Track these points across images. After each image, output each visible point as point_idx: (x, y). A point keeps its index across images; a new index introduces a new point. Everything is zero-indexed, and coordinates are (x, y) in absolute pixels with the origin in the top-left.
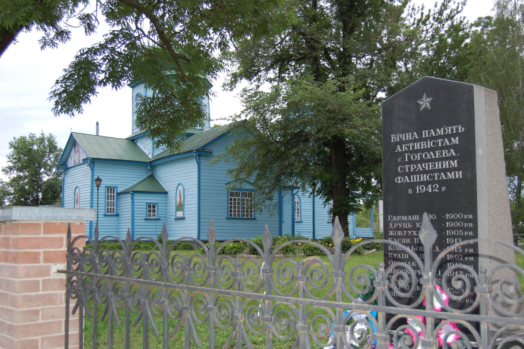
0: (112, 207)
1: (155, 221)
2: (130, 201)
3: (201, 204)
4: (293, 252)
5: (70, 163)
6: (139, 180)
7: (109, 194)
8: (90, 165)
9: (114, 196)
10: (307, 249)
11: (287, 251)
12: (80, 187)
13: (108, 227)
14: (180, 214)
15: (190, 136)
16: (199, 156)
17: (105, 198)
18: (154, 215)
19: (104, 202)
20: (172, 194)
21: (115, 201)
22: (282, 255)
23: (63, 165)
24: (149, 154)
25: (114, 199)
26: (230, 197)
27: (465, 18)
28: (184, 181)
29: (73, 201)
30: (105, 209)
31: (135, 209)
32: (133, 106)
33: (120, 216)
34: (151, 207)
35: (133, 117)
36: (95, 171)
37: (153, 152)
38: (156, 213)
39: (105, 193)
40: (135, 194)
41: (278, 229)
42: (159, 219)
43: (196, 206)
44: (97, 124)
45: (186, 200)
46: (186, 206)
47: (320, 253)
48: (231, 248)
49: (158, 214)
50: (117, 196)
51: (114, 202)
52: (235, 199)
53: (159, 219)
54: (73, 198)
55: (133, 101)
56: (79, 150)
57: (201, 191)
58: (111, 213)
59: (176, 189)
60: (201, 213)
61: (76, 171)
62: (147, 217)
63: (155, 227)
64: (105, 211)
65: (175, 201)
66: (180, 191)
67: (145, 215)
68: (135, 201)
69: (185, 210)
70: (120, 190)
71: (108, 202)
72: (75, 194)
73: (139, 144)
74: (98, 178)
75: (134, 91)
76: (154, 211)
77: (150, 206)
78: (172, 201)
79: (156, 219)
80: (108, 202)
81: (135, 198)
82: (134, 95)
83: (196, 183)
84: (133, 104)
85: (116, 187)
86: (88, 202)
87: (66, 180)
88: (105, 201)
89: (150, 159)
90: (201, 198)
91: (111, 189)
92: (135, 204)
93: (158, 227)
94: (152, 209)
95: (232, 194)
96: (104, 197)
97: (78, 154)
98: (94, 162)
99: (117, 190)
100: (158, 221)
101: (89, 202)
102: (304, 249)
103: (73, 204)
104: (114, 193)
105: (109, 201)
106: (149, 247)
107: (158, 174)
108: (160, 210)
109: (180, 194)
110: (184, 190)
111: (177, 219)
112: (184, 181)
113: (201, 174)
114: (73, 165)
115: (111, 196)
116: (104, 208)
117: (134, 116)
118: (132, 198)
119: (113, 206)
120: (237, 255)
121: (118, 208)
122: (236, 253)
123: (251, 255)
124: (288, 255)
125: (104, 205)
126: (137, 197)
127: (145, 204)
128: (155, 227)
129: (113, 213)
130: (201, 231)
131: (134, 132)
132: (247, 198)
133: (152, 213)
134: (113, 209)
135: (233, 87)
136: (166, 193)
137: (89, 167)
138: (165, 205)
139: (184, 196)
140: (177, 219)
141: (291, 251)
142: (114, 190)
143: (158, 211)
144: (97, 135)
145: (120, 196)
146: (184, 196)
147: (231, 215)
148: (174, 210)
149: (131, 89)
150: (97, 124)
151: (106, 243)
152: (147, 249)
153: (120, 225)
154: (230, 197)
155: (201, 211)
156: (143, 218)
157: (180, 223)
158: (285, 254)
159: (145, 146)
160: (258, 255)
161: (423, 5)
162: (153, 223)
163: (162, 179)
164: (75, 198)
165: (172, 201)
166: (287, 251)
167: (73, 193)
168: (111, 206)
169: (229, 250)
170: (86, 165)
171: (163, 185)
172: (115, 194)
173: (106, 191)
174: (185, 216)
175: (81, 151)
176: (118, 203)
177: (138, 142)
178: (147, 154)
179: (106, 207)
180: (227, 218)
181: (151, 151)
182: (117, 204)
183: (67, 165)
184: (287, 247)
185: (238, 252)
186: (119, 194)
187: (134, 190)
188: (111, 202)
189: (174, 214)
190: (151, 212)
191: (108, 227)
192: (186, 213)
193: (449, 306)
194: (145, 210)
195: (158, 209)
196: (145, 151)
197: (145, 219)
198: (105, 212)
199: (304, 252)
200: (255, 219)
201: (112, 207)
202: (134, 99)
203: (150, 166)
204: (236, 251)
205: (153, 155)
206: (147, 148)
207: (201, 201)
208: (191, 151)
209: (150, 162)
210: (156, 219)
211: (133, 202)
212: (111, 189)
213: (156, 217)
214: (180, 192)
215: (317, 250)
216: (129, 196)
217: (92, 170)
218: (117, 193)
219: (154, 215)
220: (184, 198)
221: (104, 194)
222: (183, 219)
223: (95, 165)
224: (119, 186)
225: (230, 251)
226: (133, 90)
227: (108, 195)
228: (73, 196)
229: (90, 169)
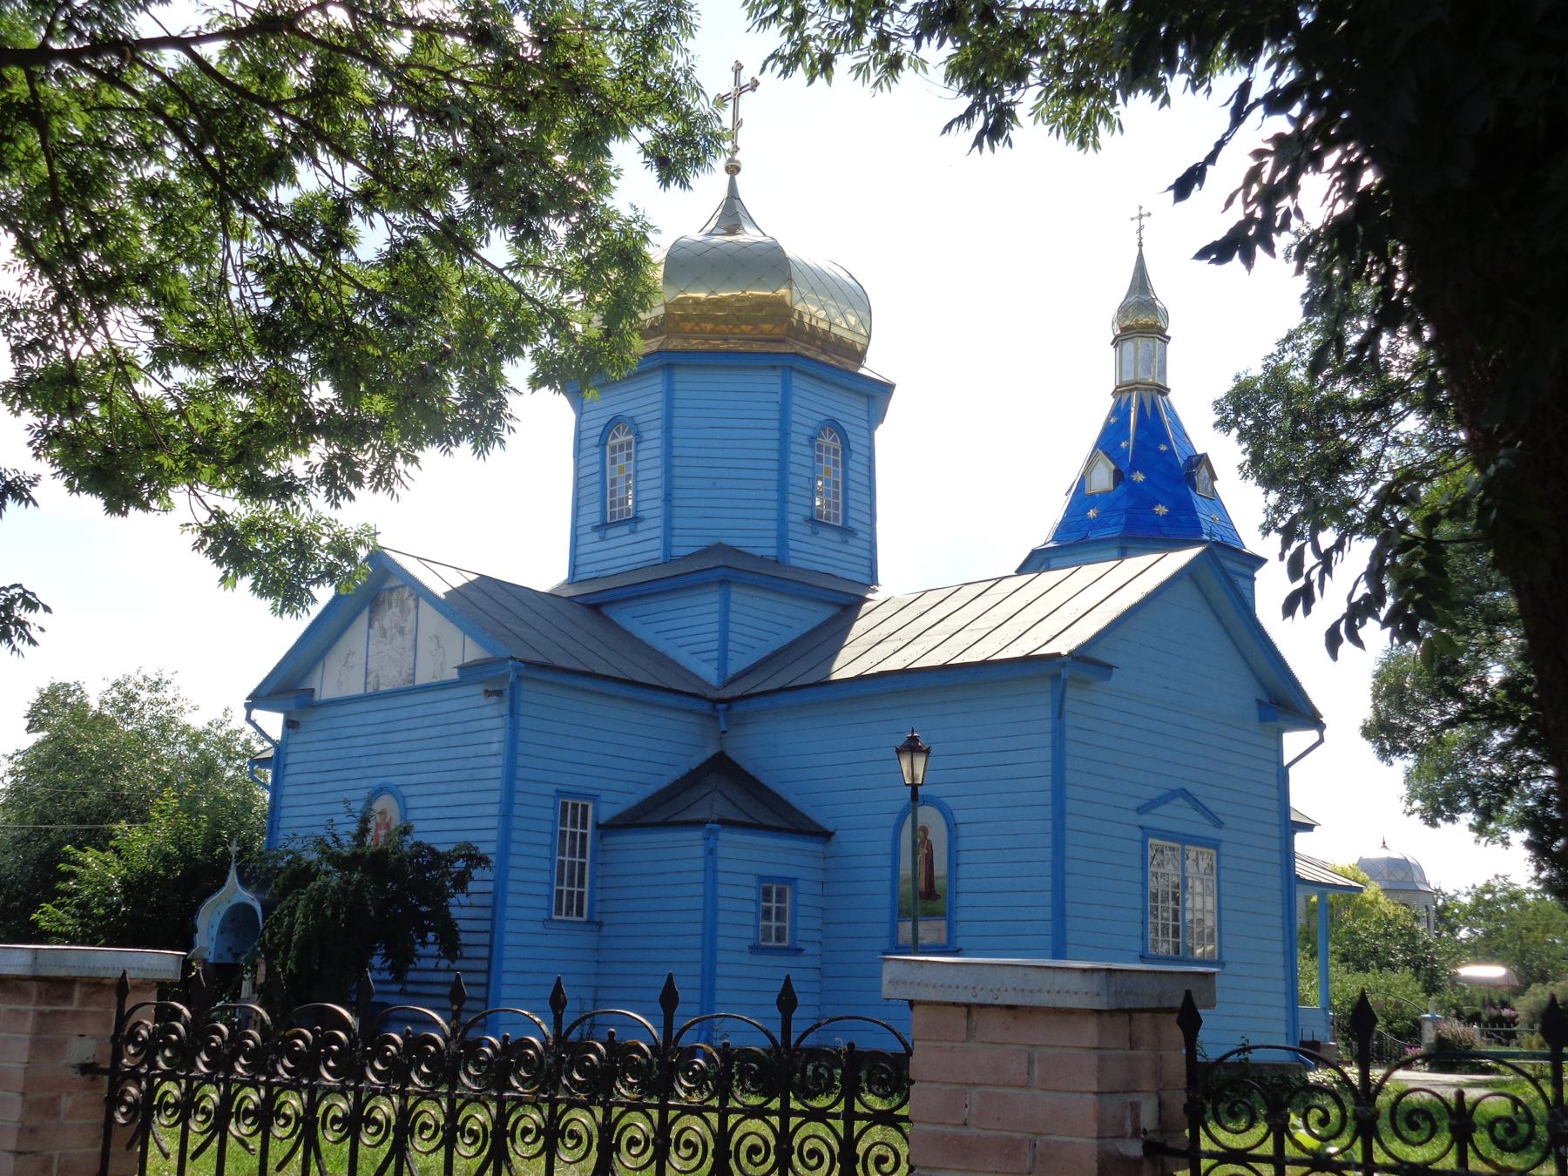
9: (584, 836)
12: (405, 791)
27: (54, 475)
34: (771, 889)
45: (963, 871)
46: (963, 900)
49: (794, 929)
53: (798, 951)
58: (567, 915)
65: (887, 873)
67: (750, 933)
69: (962, 915)
77: (767, 894)
80: (562, 863)
85: (594, 798)
86: (293, 801)
96: (547, 839)
104: (584, 826)
105: (567, 859)
110: (952, 827)
115: (573, 835)
116: (544, 890)
119: (581, 884)
127: (752, 881)
129: (580, 913)
131: (578, 578)
143: (795, 916)
148: (885, 915)
156: (744, 945)
172: (589, 831)
174: (1225, 958)
182: (594, 877)
186: (605, 829)
193: (1224, 425)
198: (549, 909)
211: (711, 870)
218: (598, 826)
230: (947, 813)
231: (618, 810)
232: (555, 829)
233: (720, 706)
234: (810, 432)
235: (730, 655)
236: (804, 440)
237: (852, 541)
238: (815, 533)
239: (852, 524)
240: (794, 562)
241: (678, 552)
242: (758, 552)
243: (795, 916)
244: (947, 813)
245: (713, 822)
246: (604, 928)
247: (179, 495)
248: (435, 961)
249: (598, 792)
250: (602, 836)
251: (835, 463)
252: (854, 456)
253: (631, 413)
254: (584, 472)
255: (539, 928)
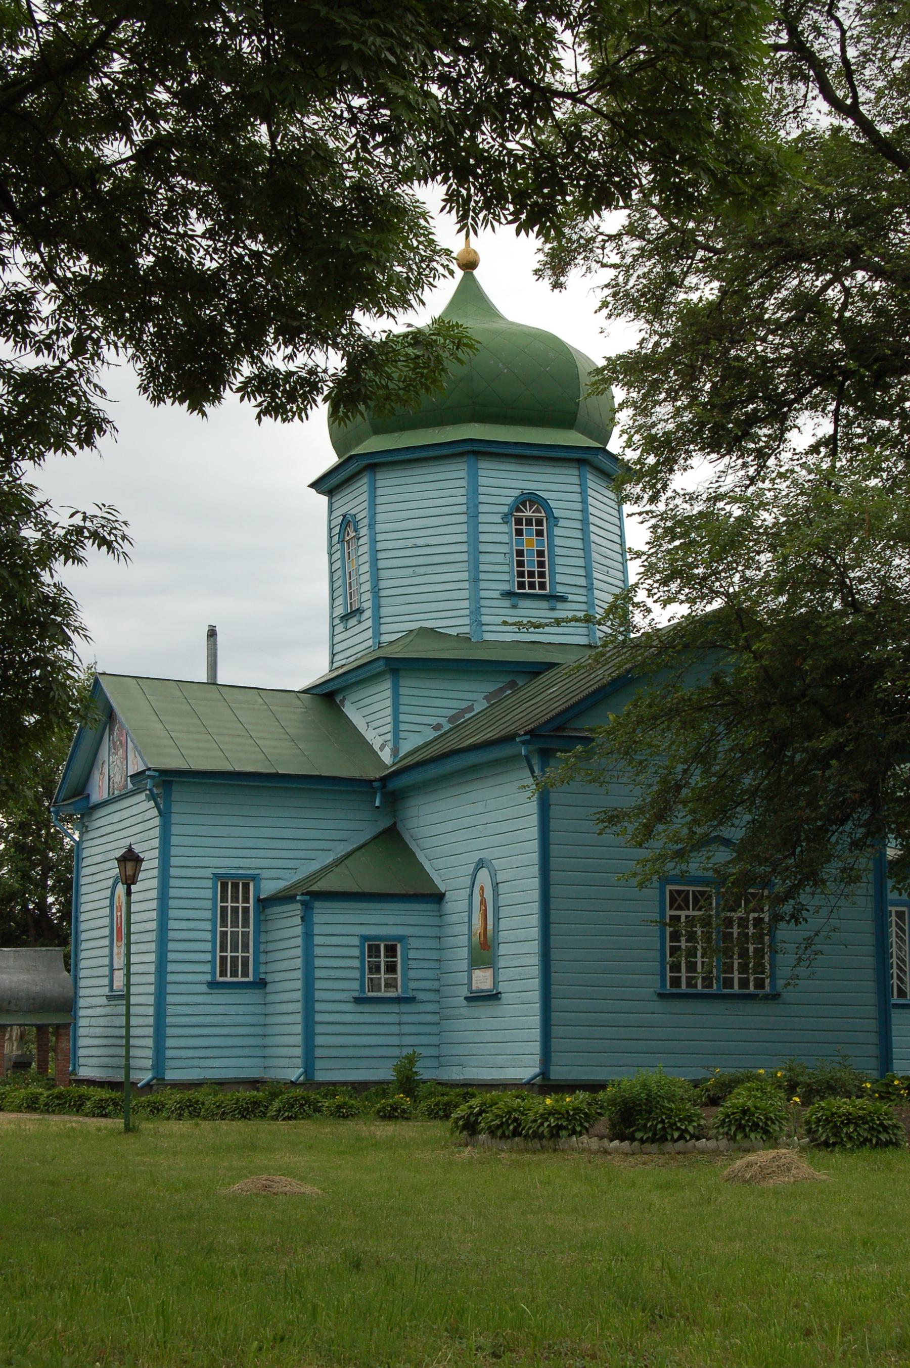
0: (240, 954)
1: (394, 1008)
2: (299, 931)
3: (554, 941)
4: (766, 1132)
5: (99, 791)
6: (342, 849)
7: (229, 904)
8: (152, 797)
9: (246, 910)
10: (819, 1120)
11: (741, 1128)
13: (225, 1031)
14: (482, 980)
15: (538, 674)
16: (546, 755)
17: (213, 921)
18: (391, 984)
19: (208, 936)
20: (456, 903)
21: (251, 929)
22: (723, 1143)
23: (74, 796)
24: (382, 748)
25: (246, 924)
26: (669, 913)
28: (496, 852)
29: (106, 932)
30: (212, 962)
31: (318, 962)
32: (331, 564)
33: (270, 988)
35: (332, 608)
36: (175, 818)
37: (397, 739)
38: (399, 975)
39: (214, 899)
40: (317, 904)
41: (873, 1038)
42: (412, 1000)
43: (535, 947)
44: (212, 633)
45: (503, 924)
46: (503, 949)
47: (866, 1134)
48: (542, 1115)
50: (258, 912)
51: (246, 935)
52: (743, 923)
53: (412, 1000)
54: (106, 921)
55: (331, 546)
56: (123, 739)
57: (554, 890)
59: (467, 881)
60: (555, 976)
61: (116, 817)
62: (362, 989)
63: (395, 1029)
64: (214, 968)
66: (482, 888)
67: (356, 985)
68: (317, 929)
69: (502, 964)
70: (269, 888)
71: (224, 934)
72: (112, 905)
73: (350, 711)
74: (130, 850)
75: (335, 506)
76: (391, 968)
77: (374, 951)
78: (458, 929)
79: (398, 1000)
81: (317, 918)
82: (333, 524)
83: (535, 858)
84: (331, 555)
85: (254, 878)
87: (85, 853)
88: (213, 931)
89: (387, 767)
90: (554, 916)
91: (235, 886)
92: (317, 940)
93: (405, 1029)
94: (383, 959)
95: (678, 900)
96: (208, 914)
97: (120, 753)
98: (171, 782)
99: (257, 889)
100: (405, 1008)
101: (153, 936)
102: (808, 1122)
103: (106, 942)
104: (246, 899)
106: (351, 1107)
107: (412, 823)
108: (413, 964)
109: (483, 902)
110: (496, 886)
111: (479, 998)
112: (496, 852)
113: (553, 824)
114: (105, 796)
115: (235, 910)
116: (208, 957)
117: (336, 603)
118: (306, 919)
119: (246, 948)
120: (562, 1143)
121: (263, 958)
122: (555, 1133)
123: (611, 1140)
124: (746, 1144)
125: (208, 946)
126: (323, 914)
127: (356, 941)
128: (395, 1029)
129: (245, 974)
130: (555, 1044)
131: (336, 665)
132: (691, 913)
133: (383, 975)
134: (246, 961)
135: (659, 486)
136: (438, 898)
137: (152, 803)
138: (434, 944)
139: (496, 909)
140: (479, 998)
141: (755, 1127)
142: (246, 887)
143: (407, 969)
144: (212, 682)
145: (269, 911)
146: (496, 909)
147: (676, 982)
148: (464, 965)
149: (324, 499)
150: (212, 633)
151: (205, 1089)
152: (345, 1117)
153: (270, 1020)
154: (669, 913)
155: (554, 966)
157: (484, 1010)
158: (733, 1138)
159: (369, 719)
160: (636, 1143)
161: (259, 423)
162: (388, 1015)
163: (426, 843)
164: (112, 919)
165: (458, 929)
166: (741, 1128)
167: (107, 903)
168: (235, 949)
169: (535, 1121)
170: (142, 796)
171: (427, 866)
172: (251, 905)
173: (215, 893)
174: (502, 987)
175: (130, 745)
176: (263, 938)
177: (347, 703)
178: (376, 748)
179: (218, 954)
180: (662, 996)
181: (389, 737)
183: (88, 796)
184: (745, 1112)
185: (565, 1128)
186: (264, 904)
187: (314, 888)
188: (235, 934)
189: (463, 978)
190: (378, 970)
191: (225, 1031)
192: (503, 975)
194: (356, 963)
195: (406, 959)
196: (370, 736)
197: (358, 1000)
199: (809, 1131)
200: (775, 997)
201: (240, 954)
202: (336, 539)
203: (384, 796)
204: (560, 1128)
205: (395, 751)
206: (375, 724)
207: (554, 929)
208: (507, 739)
209: (384, 780)
210: (398, 1000)
211: (308, 936)
212: (235, 886)
213: (399, 992)
214: (482, 896)
215: (856, 1125)
216: (296, 909)
217: (165, 815)
218: (259, 900)
219: (391, 984)
220: (497, 919)
221: (209, 904)
222: (493, 997)
223: (175, 796)
224: (265, 874)
225: (535, 1126)
226: (331, 505)
227: (224, 910)
228: (107, 911)
229: (155, 812)
230: (493, 874)
231: (281, 885)
232: (215, 905)
233: (376, 784)
234: (505, 509)
235: (402, 735)
236: (498, 519)
237: (560, 605)
238: (514, 607)
239: (560, 589)
240: (488, 637)
241: (385, 639)
242: (453, 632)
243: (407, 969)
244: (493, 874)
245: (302, 894)
246: (269, 986)
247: (877, 128)
248: (403, 1032)
249: (257, 872)
250: (264, 908)
251: (540, 533)
252: (562, 523)
253: (353, 512)
254: (334, 568)
255: (204, 989)
